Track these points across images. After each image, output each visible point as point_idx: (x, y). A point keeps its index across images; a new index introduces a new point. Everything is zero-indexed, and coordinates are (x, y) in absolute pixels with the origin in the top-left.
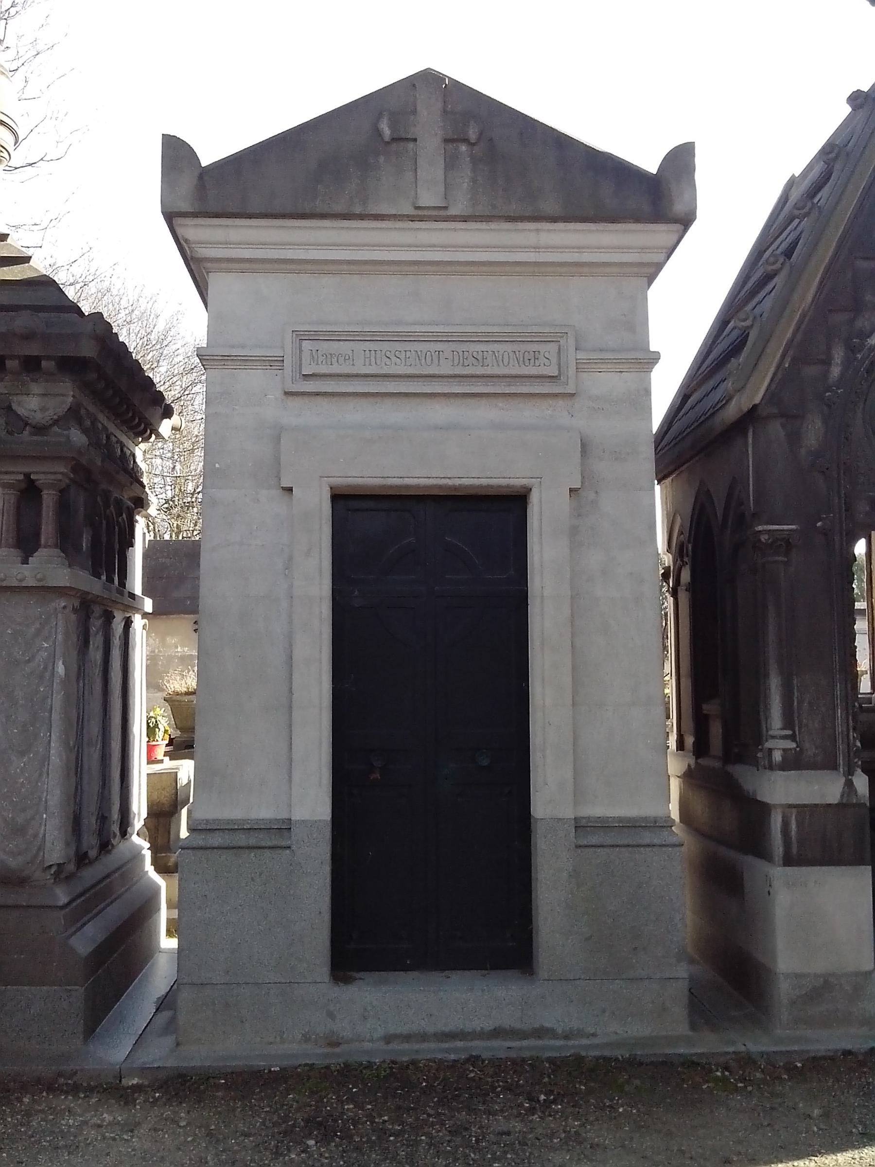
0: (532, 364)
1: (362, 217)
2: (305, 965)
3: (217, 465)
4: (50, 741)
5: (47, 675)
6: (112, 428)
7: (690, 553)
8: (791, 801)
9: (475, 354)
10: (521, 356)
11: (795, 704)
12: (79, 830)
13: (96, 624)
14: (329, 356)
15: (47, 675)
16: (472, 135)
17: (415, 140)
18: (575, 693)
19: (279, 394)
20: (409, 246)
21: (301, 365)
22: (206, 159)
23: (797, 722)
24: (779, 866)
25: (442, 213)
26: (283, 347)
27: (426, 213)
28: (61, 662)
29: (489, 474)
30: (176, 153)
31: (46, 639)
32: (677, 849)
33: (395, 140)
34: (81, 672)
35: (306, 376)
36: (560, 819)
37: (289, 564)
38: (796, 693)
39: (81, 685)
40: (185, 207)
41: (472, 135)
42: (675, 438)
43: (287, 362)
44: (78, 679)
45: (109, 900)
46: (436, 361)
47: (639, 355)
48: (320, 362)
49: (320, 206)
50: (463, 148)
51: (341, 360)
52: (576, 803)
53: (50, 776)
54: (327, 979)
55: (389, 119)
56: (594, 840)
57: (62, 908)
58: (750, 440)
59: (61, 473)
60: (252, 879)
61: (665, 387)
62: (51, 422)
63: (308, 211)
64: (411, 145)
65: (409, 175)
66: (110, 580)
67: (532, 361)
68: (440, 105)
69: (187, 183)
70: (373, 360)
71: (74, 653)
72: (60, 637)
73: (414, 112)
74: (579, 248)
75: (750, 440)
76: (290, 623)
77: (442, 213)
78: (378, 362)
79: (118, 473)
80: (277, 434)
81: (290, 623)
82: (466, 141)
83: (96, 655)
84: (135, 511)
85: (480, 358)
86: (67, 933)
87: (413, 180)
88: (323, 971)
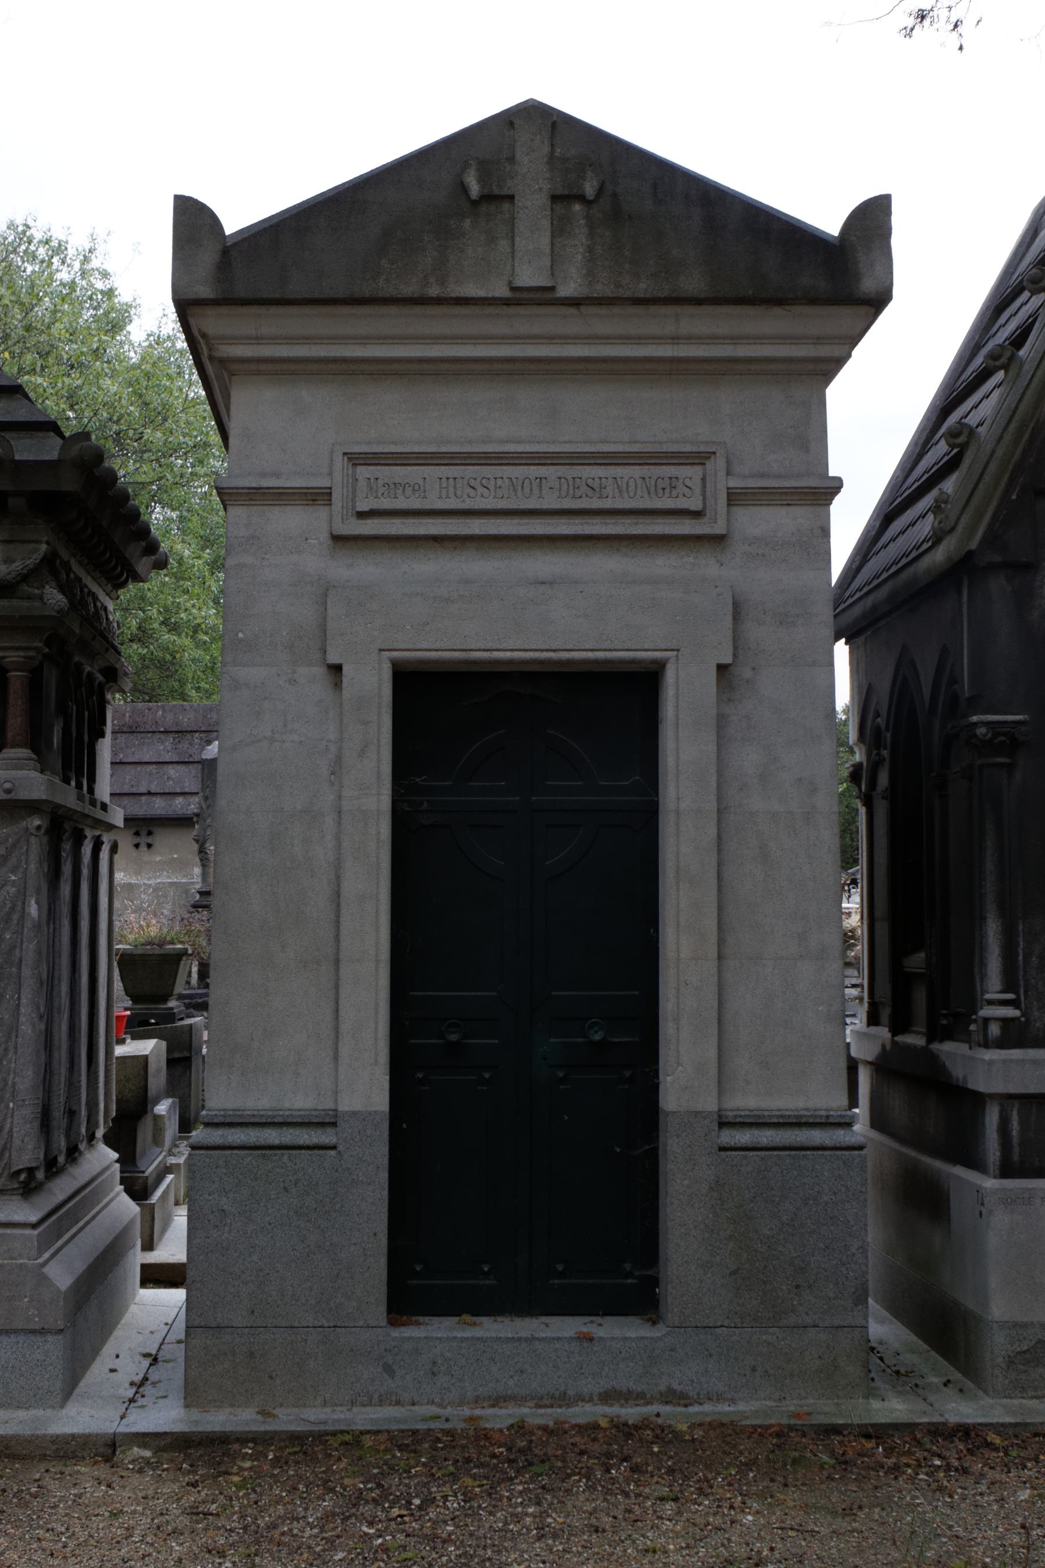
0: (667, 494)
1: (439, 301)
2: (354, 1304)
3: (240, 635)
4: (18, 1005)
5: (15, 917)
6: (81, 573)
7: (889, 746)
8: (1013, 1089)
9: (590, 481)
10: (653, 483)
11: (1021, 958)
12: (48, 1126)
13: (67, 846)
14: (392, 486)
15: (15, 917)
16: (589, 189)
17: (511, 198)
18: (721, 942)
19: (324, 536)
20: (503, 338)
21: (354, 496)
22: (231, 225)
23: (1022, 983)
24: (995, 1177)
25: (548, 295)
26: (330, 474)
27: (526, 295)
28: (33, 902)
29: (607, 645)
30: (192, 219)
31: (13, 871)
32: (856, 1153)
33: (487, 198)
34: (51, 914)
35: (362, 515)
36: (697, 1112)
37: (337, 766)
38: (1021, 943)
39: (51, 930)
40: (205, 291)
41: (589, 189)
42: (868, 583)
43: (336, 496)
44: (48, 923)
45: (87, 1219)
46: (536, 491)
47: (813, 482)
48: (380, 495)
49: (384, 287)
50: (577, 207)
51: (409, 490)
52: (720, 1093)
53: (20, 1051)
54: (384, 1323)
55: (478, 170)
56: (744, 1137)
57: (34, 1226)
58: (965, 598)
59: (35, 648)
60: (286, 1189)
61: (848, 524)
62: (19, 578)
63: (367, 295)
64: (506, 206)
65: (504, 244)
66: (79, 786)
67: (667, 491)
68: (546, 149)
69: (208, 258)
70: (451, 489)
71: (44, 888)
72: (33, 866)
73: (512, 159)
74: (732, 338)
75: (965, 598)
76: (339, 845)
77: (548, 295)
78: (459, 493)
79: (93, 639)
80: (325, 591)
81: (339, 845)
82: (581, 198)
83: (65, 889)
84: (107, 686)
85: (596, 486)
86: (40, 1261)
87: (509, 250)
88: (379, 1311)
